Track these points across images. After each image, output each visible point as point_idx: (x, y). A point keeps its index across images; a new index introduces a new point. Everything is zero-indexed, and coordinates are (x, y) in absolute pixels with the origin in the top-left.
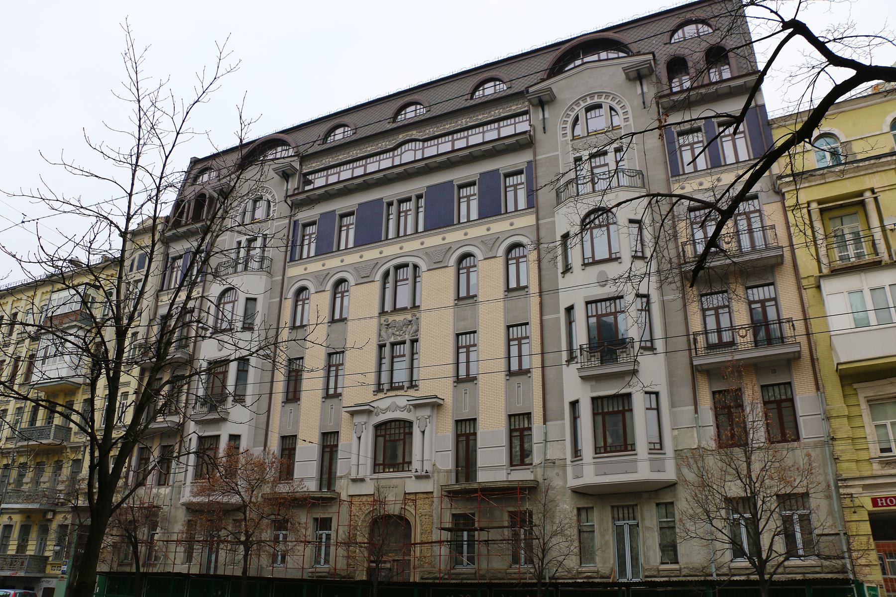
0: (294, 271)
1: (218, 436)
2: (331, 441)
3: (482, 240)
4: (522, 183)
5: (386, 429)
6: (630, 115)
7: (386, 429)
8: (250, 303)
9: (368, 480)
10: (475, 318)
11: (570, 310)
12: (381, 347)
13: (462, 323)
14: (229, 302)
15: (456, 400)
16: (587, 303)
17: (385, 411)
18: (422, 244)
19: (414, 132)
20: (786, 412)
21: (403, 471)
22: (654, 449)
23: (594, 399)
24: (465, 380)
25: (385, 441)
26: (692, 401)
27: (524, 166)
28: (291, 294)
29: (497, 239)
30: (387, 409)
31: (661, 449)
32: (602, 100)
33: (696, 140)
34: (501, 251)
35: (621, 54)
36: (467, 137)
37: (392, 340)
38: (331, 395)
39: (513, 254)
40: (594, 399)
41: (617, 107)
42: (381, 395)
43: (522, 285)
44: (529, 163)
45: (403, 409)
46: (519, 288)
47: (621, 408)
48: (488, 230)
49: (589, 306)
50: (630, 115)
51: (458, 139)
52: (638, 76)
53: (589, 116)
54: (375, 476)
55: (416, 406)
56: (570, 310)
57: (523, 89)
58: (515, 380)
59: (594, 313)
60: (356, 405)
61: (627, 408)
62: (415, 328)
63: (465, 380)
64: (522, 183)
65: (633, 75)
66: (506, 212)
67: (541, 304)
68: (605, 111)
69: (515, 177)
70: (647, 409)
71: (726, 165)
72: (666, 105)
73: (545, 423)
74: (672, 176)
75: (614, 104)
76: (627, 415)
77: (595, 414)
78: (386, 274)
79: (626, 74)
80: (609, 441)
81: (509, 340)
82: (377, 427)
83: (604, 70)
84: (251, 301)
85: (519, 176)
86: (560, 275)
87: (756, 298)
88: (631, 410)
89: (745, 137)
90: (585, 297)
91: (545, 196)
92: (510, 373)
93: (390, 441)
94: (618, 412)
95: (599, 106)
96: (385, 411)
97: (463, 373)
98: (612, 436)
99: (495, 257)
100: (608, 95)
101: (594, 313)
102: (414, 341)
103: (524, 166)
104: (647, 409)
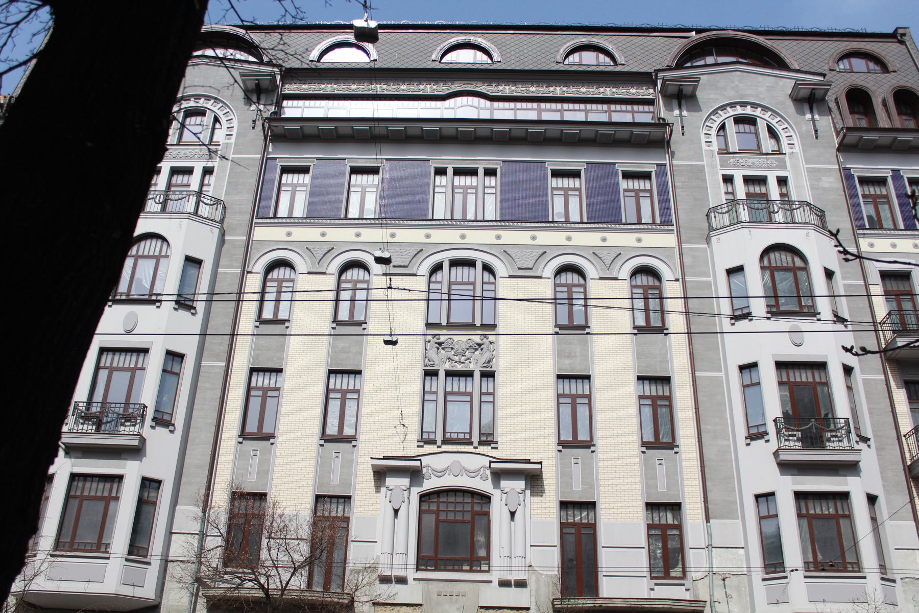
1: (120, 478)
3: (308, 248)
4: (305, 185)
5: (438, 503)
7: (438, 503)
8: (736, 279)
9: (410, 580)
10: (586, 356)
13: (567, 361)
14: (148, 257)
15: (564, 476)
17: (441, 473)
23: (74, 477)
24: (576, 442)
25: (438, 521)
28: (259, 266)
29: (330, 250)
32: (208, 106)
33: (301, 182)
34: (334, 267)
35: (251, 59)
37: (448, 366)
38: (337, 438)
39: (275, 274)
40: (74, 477)
41: (223, 119)
43: (356, 318)
46: (276, 321)
47: (106, 494)
51: (616, 111)
52: (810, 100)
54: (421, 575)
58: (250, 445)
59: (108, 365)
60: (385, 458)
62: (487, 356)
63: (576, 442)
64: (305, 185)
65: (251, 85)
66: (275, 217)
67: (692, 355)
68: (208, 119)
69: (296, 176)
71: (433, 220)
72: (277, 131)
73: (708, 520)
74: (257, 217)
75: (220, 114)
76: (112, 504)
78: (438, 267)
80: (820, 557)
81: (328, 391)
82: (425, 497)
83: (760, 78)
84: (193, 262)
85: (301, 176)
88: (117, 498)
89: (580, 196)
92: (326, 438)
93: (447, 521)
94: (101, 498)
95: (201, 113)
96: (441, 473)
97: (332, 430)
98: (822, 554)
99: (324, 273)
100: (765, 109)
101: (108, 365)
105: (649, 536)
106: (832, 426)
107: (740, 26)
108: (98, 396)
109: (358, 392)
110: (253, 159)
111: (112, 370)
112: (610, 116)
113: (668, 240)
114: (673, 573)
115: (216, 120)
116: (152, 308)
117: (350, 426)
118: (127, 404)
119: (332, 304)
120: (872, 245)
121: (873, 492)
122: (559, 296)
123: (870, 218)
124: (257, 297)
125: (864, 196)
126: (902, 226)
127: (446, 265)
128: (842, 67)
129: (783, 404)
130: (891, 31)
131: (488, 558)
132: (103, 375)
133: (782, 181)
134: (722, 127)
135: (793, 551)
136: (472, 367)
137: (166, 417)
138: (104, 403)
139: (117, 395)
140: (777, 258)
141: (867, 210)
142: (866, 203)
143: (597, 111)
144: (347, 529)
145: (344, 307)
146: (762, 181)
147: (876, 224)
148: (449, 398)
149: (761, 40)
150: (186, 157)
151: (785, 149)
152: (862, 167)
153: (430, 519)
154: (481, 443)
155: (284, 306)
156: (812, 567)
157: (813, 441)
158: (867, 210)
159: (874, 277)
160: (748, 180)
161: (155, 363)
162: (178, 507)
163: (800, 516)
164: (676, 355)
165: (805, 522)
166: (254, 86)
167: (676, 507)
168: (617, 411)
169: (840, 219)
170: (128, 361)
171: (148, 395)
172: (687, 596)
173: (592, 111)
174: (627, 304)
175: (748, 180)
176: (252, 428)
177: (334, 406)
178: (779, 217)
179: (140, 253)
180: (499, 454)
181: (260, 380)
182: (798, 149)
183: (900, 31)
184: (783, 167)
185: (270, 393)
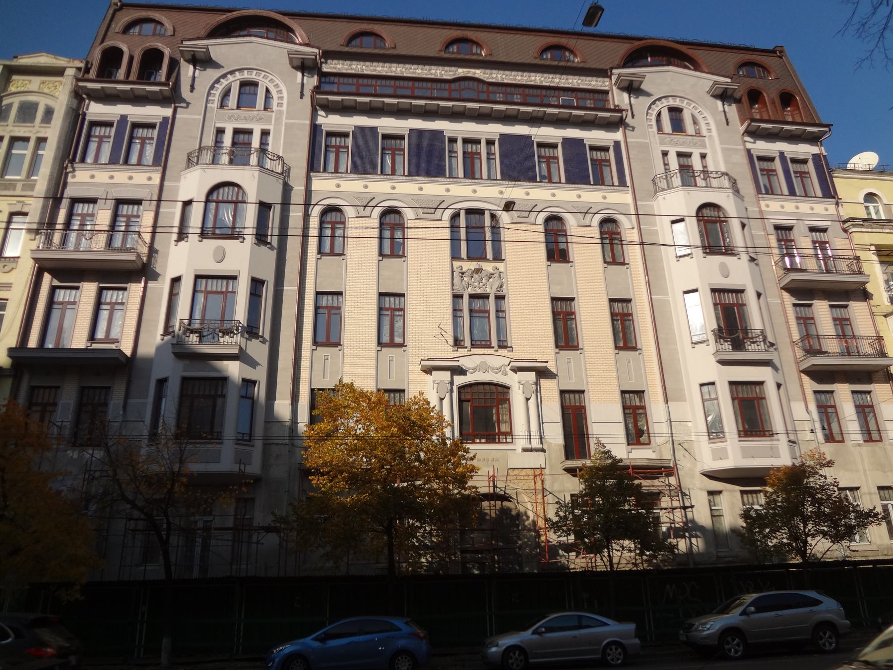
0: (322, 184)
2: (571, 399)
6: (285, 102)
11: (176, 281)
12: (457, 297)
16: (198, 277)
18: (338, 186)
19: (478, 71)
20: (870, 417)
21: (499, 442)
22: (243, 440)
23: (184, 379)
26: (801, 397)
27: (158, 121)
28: (316, 211)
30: (475, 370)
31: (250, 440)
32: (261, 78)
34: (377, 212)
36: (375, 86)
37: (470, 290)
40: (184, 379)
42: (462, 352)
44: (165, 119)
45: (498, 370)
47: (213, 393)
48: (131, 178)
49: (199, 280)
50: (285, 102)
51: (344, 84)
53: (242, 91)
55: (516, 370)
56: (176, 281)
57: (608, 67)
61: (219, 393)
67: (648, 283)
70: (242, 397)
76: (219, 401)
77: (182, 396)
79: (291, 59)
86: (173, 243)
87: (387, 306)
88: (223, 396)
90: (195, 270)
91: (177, 156)
96: (475, 370)
97: (386, 339)
102: (500, 298)
103: (351, 130)
104: (242, 397)
105: (625, 414)
106: (750, 335)
107: (666, 37)
108: (197, 315)
109: (402, 310)
110: (303, 124)
111: (207, 293)
112: (488, 96)
113: (624, 198)
114: (642, 439)
115: (267, 91)
116: (236, 242)
117: (399, 336)
118: (222, 320)
119: (376, 241)
120: (768, 206)
121: (780, 382)
122: (342, 231)
123: (765, 186)
124: (300, 232)
125: (761, 170)
126: (563, 180)
127: (463, 213)
128: (741, 73)
129: (718, 318)
130: (771, 48)
131: (510, 433)
132: (201, 297)
133: (703, 156)
134: (659, 115)
135: (730, 423)
136: (488, 290)
137: (505, 344)
138: (203, 320)
139: (214, 314)
140: (706, 212)
141: (763, 180)
142: (796, 177)
143: (422, 88)
144: (628, 434)
145: (327, 242)
146: (689, 155)
147: (770, 191)
148: (475, 315)
149: (683, 48)
150: (246, 119)
151: (704, 132)
152: (762, 147)
153: (468, 406)
154: (500, 347)
155: (338, 241)
156: (742, 433)
157: (738, 345)
158: (763, 180)
159: (771, 230)
160: (680, 155)
161: (243, 289)
162: (131, 401)
163: (733, 399)
164: (634, 281)
165: (736, 402)
166: (190, 57)
167: (640, 393)
168: (593, 323)
169: (747, 186)
170: (220, 285)
171: (240, 314)
172: (653, 456)
173: (363, 85)
174: (812, 252)
175: (680, 155)
176: (386, 339)
177: (386, 321)
178: (700, 181)
179: (220, 198)
180: (515, 355)
181: (325, 301)
182: (714, 133)
183: (779, 49)
184: (704, 146)
185: (117, 307)
